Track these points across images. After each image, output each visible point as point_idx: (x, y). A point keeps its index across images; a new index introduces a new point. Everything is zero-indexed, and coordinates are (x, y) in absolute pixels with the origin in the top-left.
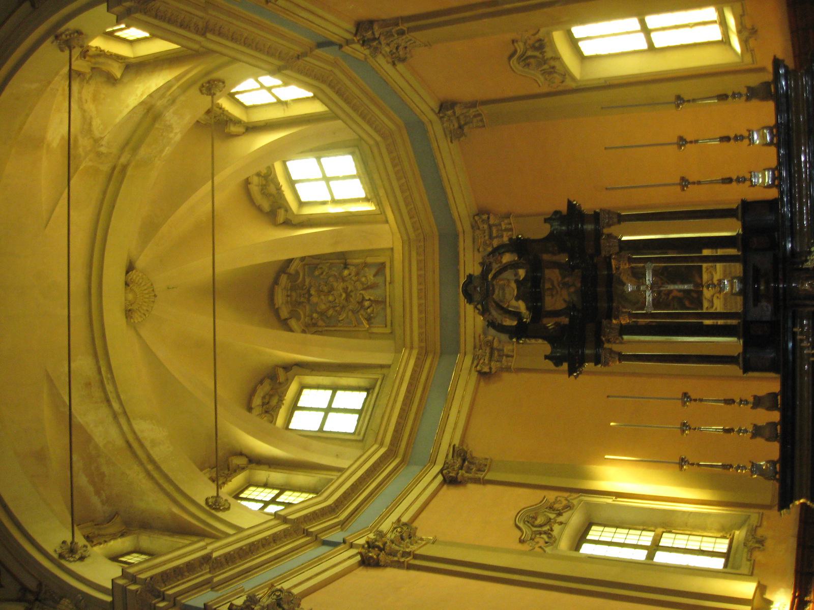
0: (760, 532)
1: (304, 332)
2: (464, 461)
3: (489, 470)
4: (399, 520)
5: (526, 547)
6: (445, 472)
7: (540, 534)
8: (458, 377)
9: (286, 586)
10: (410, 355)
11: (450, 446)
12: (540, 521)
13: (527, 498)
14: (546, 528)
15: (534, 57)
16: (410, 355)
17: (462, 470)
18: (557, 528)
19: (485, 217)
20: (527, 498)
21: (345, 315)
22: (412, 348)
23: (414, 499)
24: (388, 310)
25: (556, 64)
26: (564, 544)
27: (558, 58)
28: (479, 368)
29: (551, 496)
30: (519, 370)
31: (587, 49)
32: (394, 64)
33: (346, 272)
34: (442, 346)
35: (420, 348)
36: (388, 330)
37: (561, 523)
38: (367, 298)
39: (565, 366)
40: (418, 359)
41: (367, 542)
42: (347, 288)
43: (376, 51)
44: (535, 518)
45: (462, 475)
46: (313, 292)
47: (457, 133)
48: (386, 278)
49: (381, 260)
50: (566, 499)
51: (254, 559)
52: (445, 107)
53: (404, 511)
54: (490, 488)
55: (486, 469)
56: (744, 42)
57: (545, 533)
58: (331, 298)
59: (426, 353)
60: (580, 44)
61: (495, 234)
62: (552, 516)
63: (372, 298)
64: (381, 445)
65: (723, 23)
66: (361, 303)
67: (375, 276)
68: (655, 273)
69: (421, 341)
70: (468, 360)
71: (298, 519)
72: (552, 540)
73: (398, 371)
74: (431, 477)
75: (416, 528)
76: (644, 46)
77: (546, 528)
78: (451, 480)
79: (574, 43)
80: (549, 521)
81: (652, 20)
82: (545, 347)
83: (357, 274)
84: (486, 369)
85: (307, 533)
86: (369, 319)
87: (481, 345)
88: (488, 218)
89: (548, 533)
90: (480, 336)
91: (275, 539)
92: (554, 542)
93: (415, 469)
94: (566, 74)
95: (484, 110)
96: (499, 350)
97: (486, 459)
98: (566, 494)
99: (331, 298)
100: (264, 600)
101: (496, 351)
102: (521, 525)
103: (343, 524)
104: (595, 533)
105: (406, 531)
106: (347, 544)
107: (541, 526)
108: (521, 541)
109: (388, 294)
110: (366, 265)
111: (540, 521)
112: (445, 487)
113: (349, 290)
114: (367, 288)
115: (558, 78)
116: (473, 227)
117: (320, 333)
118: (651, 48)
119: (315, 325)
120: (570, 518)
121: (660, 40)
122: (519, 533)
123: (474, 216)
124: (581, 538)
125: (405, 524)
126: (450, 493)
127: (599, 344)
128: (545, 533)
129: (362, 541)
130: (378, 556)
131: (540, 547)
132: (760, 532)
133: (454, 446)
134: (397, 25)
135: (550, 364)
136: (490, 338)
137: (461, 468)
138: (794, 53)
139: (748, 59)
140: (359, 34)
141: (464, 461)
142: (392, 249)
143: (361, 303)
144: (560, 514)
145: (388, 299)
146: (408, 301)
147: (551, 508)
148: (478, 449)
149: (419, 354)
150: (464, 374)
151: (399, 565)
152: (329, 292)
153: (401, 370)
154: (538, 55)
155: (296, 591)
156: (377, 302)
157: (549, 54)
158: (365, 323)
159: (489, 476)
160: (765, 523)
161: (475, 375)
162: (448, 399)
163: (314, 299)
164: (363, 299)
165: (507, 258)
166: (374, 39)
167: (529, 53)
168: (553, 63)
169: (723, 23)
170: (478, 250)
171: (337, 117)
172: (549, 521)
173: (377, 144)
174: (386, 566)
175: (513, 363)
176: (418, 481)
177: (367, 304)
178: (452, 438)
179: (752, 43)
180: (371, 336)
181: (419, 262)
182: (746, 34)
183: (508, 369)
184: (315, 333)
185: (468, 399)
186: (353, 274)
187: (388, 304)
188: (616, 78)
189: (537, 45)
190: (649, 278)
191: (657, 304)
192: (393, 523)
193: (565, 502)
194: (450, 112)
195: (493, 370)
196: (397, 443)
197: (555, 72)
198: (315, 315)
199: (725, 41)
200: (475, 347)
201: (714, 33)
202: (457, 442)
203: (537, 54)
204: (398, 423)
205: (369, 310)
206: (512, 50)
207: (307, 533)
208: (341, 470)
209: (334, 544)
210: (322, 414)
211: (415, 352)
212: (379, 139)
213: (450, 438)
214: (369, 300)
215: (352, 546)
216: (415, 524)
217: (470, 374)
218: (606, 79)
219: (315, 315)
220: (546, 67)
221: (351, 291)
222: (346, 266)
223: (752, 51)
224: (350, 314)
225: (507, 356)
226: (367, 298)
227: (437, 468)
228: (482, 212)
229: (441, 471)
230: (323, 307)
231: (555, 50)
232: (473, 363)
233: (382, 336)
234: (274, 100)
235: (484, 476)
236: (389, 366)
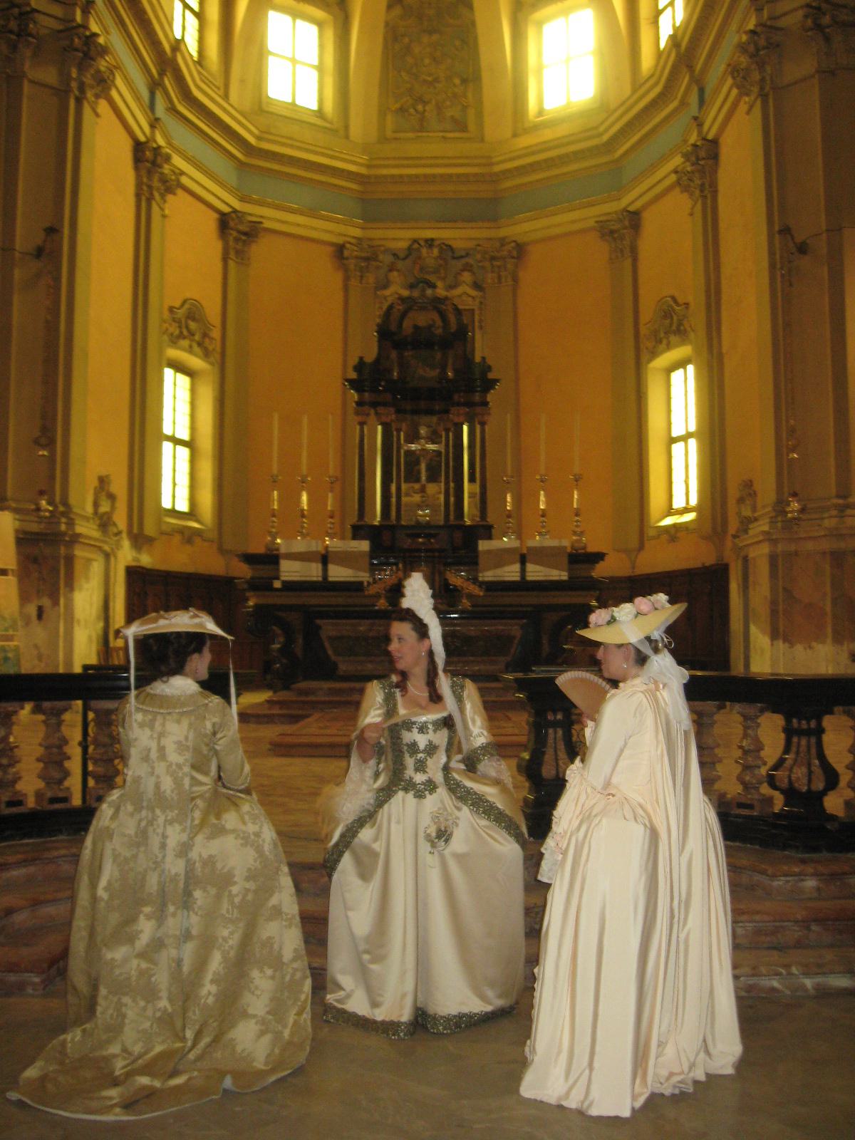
0: (198, 540)
1: (387, 24)
2: (245, 234)
3: (236, 262)
4: (182, 173)
5: (166, 315)
6: (233, 215)
7: (180, 327)
8: (338, 221)
9: (119, 81)
10: (361, 165)
11: (261, 217)
12: (193, 325)
13: (212, 311)
14: (185, 333)
15: (671, 324)
16: (361, 165)
17: (236, 233)
18: (185, 343)
19: (515, 254)
20: (212, 311)
21: (406, 78)
22: (368, 167)
23: (204, 182)
24: (410, 135)
25: (663, 345)
26: (172, 353)
27: (669, 347)
28: (348, 246)
29: (216, 334)
30: (346, 289)
31: (677, 376)
32: (676, 172)
33: (457, 81)
34: (373, 196)
35: (368, 177)
36: (389, 133)
37: (191, 347)
38: (427, 108)
39: (353, 375)
40: (357, 174)
41: (159, 147)
42: (438, 82)
43: (686, 156)
44: (194, 319)
45: (231, 234)
46: (435, 37)
47: (607, 231)
48: (451, 132)
49: (472, 126)
50: (214, 350)
51: (133, 26)
52: (634, 219)
53: (193, 177)
54: (220, 265)
55: (239, 260)
56: (667, 529)
57: (181, 332)
58: (427, 61)
59: (361, 183)
60: (681, 370)
61: (496, 263)
62: (197, 337)
63: (426, 114)
64: (259, 138)
65: (686, 510)
66: (421, 100)
67: (452, 117)
68: (438, 453)
69: (377, 177)
70: (357, 232)
71: (178, 65)
72: (174, 341)
73: (342, 153)
74: (228, 201)
75: (175, 194)
76: (675, 434)
77: (185, 333)
78: (225, 222)
79: (682, 364)
80: (192, 334)
81: (693, 443)
82: (371, 355)
83: (455, 95)
84: (346, 253)
85: (162, 73)
86: (402, 110)
87: (373, 247)
88: (513, 258)
89: (181, 336)
90: (383, 246)
91: (154, 42)
92: (173, 342)
93: (232, 179)
94: (654, 354)
95: (628, 263)
96: (367, 267)
97: (249, 259)
98: (219, 349)
99: (427, 61)
100: (103, 63)
101: (366, 264)
102: (187, 306)
103: (172, 110)
104: (184, 381)
105: (171, 186)
106: (154, 123)
107: (187, 327)
108: (171, 309)
109: (431, 134)
110: (465, 108)
111: (193, 325)
112: (215, 216)
113: (437, 85)
114: (439, 108)
115: (650, 344)
116: (504, 239)
117: (385, 46)
118: (673, 440)
119: (395, 39)
120: (196, 355)
121: (677, 448)
122: (177, 304)
123: (515, 241)
124: (180, 368)
125: (178, 181)
126: (211, 221)
127: (374, 405)
128: (181, 332)
129: (161, 141)
130: (147, 161)
131: (167, 329)
132: (198, 540)
133: (261, 223)
134: (711, 187)
135: (353, 361)
136: (381, 257)
137: (239, 232)
138: (692, 569)
139: (652, 533)
140: (704, 142)
141: (245, 234)
142: (482, 140)
143: (421, 100)
144: (199, 344)
145: (424, 134)
146: (423, 162)
147: (205, 335)
148: (260, 250)
149: (362, 175)
150: (341, 228)
151: (139, 185)
152: (434, 59)
153: (343, 156)
154: (671, 325)
155: (114, 93)
156: (422, 119)
157: (673, 339)
158: (398, 106)
159: (231, 264)
160: (206, 544)
161: (340, 240)
162: (312, 212)
163: (425, 39)
164: (425, 103)
165: (452, 318)
166: (698, 159)
167: (675, 318)
168: (665, 341)
169: (686, 510)
170: (479, 245)
171: (634, 90)
172: (192, 334)
173: (600, 135)
174: (137, 168)
175: (354, 282)
176: (222, 184)
177: (420, 107)
178: (269, 219)
179: (665, 537)
180: (382, 114)
181: (467, 175)
182: (673, 532)
183: (347, 279)
184: (385, 39)
185: (314, 235)
186: (456, 90)
187: (420, 134)
188: (646, 404)
189: (682, 328)
190: (431, 447)
191: (409, 453)
192: (420, 795)
193: (211, 348)
194: (627, 223)
195: (345, 262)
196: (263, 156)
197: (656, 342)
198: (406, 40)
199: (670, 511)
200: (370, 239)
201: (678, 503)
202: (267, 224)
203: (674, 327)
204: (283, 156)
205: (412, 110)
206: (680, 301)
207: (162, 73)
208: (226, 96)
209: (152, 107)
210: (291, 56)
211: (363, 171)
212: (605, 138)
213: (270, 216)
214: (425, 111)
215: (152, 127)
216: (179, 191)
217: (340, 234)
218: (646, 394)
219: (406, 40)
220: (662, 335)
221: (435, 88)
222: (464, 81)
223: (659, 536)
224: (409, 86)
225: (362, 277)
226: (427, 108)
227: (237, 204)
228: (520, 251)
229: (235, 211)
230: (417, 50)
231: (676, 346)
232: (354, 238)
233: (382, 127)
234: (660, 7)
235: (232, 259)
236: (347, 137)
